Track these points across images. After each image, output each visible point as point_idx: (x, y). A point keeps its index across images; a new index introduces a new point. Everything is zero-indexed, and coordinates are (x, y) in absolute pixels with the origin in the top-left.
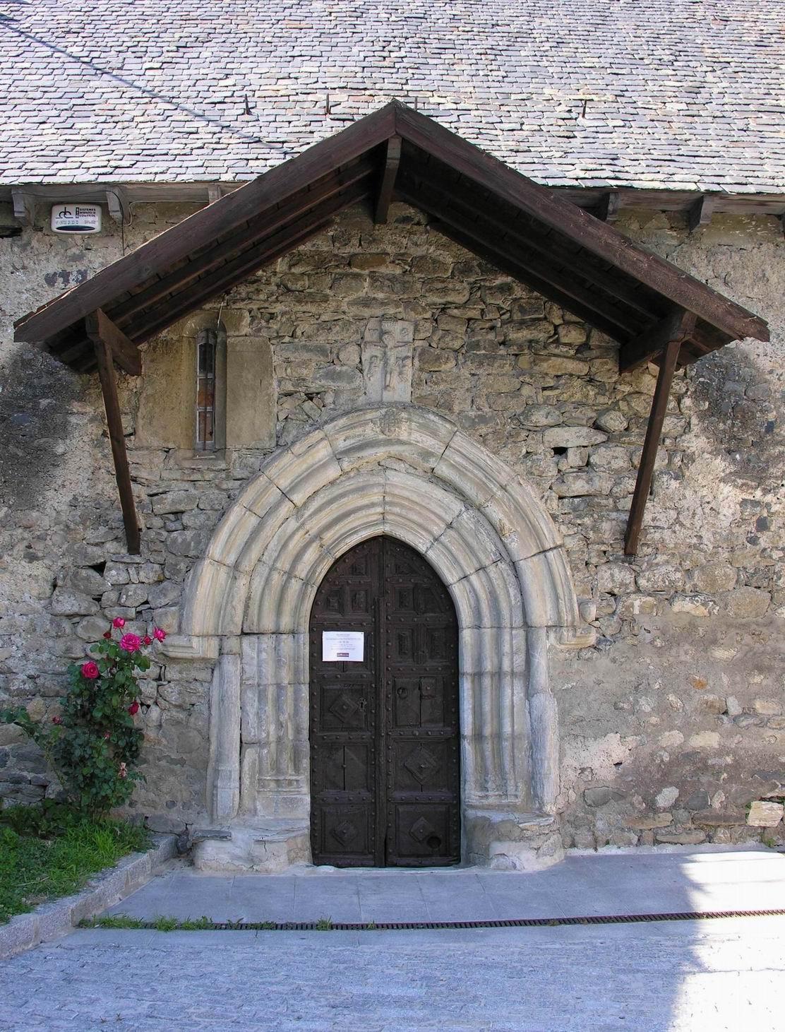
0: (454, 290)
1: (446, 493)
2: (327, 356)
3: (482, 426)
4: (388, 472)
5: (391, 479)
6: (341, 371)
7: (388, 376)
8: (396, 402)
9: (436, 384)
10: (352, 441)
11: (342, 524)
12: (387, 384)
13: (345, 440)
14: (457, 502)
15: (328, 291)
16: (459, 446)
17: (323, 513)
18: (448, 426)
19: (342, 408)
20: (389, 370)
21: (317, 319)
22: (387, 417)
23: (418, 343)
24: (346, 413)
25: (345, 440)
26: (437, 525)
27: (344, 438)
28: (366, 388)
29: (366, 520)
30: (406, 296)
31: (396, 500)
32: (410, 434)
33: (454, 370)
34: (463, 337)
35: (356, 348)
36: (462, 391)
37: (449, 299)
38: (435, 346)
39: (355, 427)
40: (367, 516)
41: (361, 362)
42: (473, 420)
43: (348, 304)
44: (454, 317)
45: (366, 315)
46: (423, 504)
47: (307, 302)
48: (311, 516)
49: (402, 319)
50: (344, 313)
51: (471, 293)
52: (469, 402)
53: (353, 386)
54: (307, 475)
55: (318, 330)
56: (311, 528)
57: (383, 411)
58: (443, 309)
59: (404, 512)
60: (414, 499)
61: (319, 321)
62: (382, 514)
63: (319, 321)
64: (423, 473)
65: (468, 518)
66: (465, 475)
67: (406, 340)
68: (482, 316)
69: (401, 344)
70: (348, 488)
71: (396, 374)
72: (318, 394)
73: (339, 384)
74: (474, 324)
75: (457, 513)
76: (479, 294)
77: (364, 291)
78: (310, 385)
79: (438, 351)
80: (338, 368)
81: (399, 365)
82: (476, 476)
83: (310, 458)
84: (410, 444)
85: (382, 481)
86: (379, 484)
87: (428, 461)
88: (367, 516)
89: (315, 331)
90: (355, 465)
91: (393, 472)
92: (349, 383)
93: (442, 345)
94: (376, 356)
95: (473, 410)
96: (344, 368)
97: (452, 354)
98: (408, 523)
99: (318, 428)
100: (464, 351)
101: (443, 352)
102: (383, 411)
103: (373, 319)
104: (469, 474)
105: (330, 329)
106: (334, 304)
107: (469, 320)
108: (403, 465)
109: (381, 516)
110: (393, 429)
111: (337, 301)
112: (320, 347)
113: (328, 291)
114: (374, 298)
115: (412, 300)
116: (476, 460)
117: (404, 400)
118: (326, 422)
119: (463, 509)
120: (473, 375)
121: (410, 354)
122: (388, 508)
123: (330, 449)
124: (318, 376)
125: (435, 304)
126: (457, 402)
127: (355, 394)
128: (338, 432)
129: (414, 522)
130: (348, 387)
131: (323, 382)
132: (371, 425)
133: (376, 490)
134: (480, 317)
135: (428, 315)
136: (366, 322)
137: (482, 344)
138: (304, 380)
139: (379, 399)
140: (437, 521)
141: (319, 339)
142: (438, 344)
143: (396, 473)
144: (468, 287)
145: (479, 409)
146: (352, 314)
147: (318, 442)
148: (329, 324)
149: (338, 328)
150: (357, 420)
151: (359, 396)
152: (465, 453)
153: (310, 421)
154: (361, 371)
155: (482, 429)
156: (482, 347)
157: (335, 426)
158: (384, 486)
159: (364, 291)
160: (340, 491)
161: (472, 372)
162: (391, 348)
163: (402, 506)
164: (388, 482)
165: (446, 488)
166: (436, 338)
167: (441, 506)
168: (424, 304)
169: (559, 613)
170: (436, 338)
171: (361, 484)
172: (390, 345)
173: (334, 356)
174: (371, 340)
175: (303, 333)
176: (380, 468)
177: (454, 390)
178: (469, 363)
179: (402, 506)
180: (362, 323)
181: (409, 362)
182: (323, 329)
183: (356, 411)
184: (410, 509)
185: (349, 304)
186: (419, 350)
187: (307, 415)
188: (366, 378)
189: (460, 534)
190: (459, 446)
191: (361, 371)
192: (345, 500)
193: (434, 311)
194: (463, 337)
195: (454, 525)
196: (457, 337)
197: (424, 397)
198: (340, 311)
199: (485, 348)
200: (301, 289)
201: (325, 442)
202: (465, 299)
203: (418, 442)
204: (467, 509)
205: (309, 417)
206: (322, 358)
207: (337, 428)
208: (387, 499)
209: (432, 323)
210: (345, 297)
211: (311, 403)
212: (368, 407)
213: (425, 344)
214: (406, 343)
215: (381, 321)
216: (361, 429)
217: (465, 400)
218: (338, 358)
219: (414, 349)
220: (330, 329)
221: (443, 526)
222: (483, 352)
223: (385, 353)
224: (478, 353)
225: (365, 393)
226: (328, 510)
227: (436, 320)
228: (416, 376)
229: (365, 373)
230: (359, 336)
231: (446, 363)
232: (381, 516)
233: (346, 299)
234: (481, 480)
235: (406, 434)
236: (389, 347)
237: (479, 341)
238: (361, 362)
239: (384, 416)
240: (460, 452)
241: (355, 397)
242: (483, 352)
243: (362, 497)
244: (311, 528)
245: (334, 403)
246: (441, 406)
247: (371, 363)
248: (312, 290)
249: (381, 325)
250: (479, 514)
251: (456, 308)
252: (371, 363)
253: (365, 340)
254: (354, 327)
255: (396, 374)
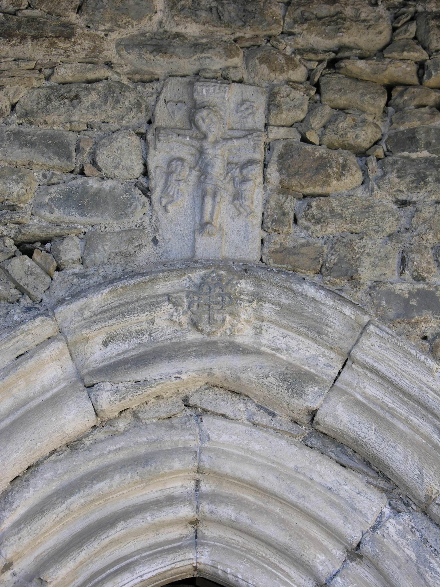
0: (356, 19)
1: (344, 472)
2: (69, 157)
3: (427, 314)
4: (207, 422)
5: (214, 436)
6: (98, 193)
7: (209, 200)
8: (226, 260)
9: (318, 221)
10: (123, 346)
11: (94, 546)
12: (207, 218)
13: (105, 344)
14: (369, 493)
15: (73, 17)
16: (375, 359)
17: (49, 519)
18: (347, 311)
19: (102, 272)
20: (209, 188)
21: (48, 78)
22: (205, 289)
23: (275, 133)
24: (108, 281)
25: (105, 344)
26: (325, 550)
27: (102, 337)
28: (156, 230)
29: (152, 539)
30: (248, 33)
31: (227, 490)
32: (258, 331)
33: (360, 192)
34: (379, 123)
35: (136, 140)
36: (379, 239)
37: (346, 39)
38: (313, 137)
39: (129, 312)
40: (157, 527)
41: (145, 174)
42: (407, 301)
43: (118, 45)
44: (357, 79)
45: (160, 72)
46: (292, 498)
47: (24, 37)
48: (18, 525)
49: (241, 82)
50: (109, 64)
51: (394, 29)
52: (394, 261)
53: (128, 223)
54: (14, 423)
55: (49, 100)
56: (20, 556)
57: (196, 276)
58: (333, 64)
59: (245, 518)
60: (266, 484)
61: (53, 82)
62: (194, 523)
63: (53, 82)
64: (291, 425)
65: (398, 532)
66: (390, 427)
67: (250, 123)
68: (420, 78)
69: (236, 133)
70: (111, 459)
71: (225, 197)
72: (44, 242)
73: (95, 220)
74: (401, 94)
75: (371, 520)
76: (413, 28)
77: (156, 18)
78: (26, 219)
79: (322, 151)
80: (93, 184)
81: (233, 179)
82: (416, 429)
83: (22, 383)
84: (259, 353)
85: (193, 443)
86: (186, 450)
87: (301, 394)
88: (157, 527)
89: (43, 103)
90: (125, 404)
91: (220, 422)
92: (118, 218)
93: (330, 137)
94: (181, 160)
95: (404, 281)
96: (108, 184)
97: (353, 159)
98: (254, 546)
99: (41, 315)
100: (380, 151)
101: (334, 153)
102: (196, 276)
103: (174, 80)
104: (400, 426)
105: (77, 97)
106: (87, 44)
107: (389, 88)
108: (241, 406)
109: (190, 530)
110: (218, 317)
111: (94, 38)
112: (52, 137)
113: (73, 17)
114: (178, 35)
115: (263, 43)
116: (415, 392)
117: (245, 257)
118: (62, 301)
119: (387, 511)
120: (403, 204)
121: (259, 156)
122: (206, 507)
123: (70, 366)
124: (46, 199)
125: (314, 51)
126: (367, 261)
127: (131, 241)
128: (90, 323)
129: (268, 543)
130: (115, 226)
131: (58, 214)
132: (168, 307)
133: (177, 465)
134: (415, 80)
135: (299, 74)
136: (157, 85)
137: (421, 136)
138: (13, 208)
139: (186, 253)
140: (326, 542)
141: (50, 119)
142: (321, 137)
143: (225, 423)
144: (387, 15)
145: (418, 278)
146: (127, 69)
147: (41, 346)
148: (74, 87)
149: (94, 97)
150: (133, 295)
151: (140, 247)
152: (389, 374)
153: (26, 302)
154: (146, 191)
155: (426, 321)
156: (422, 143)
157: (81, 310)
158: (196, 454)
159: (156, 18)
160: (92, 466)
161: (402, 197)
162: (216, 142)
163: (240, 504)
164: (207, 445)
165: (344, 460)
166: (316, 122)
167: (332, 504)
168: (289, 51)
169: (343, 545)
170: (316, 122)
171: (142, 451)
172: (214, 132)
173: (85, 157)
174: (172, 124)
175: (13, 107)
176: (189, 412)
177: (361, 236)
178: (393, 176)
179: (240, 504)
180: (149, 88)
181: (256, 171)
182: (61, 97)
183: (132, 277)
184: (261, 511)
185: (120, 45)
186: (279, 147)
187: (18, 287)
188: (157, 206)
189: (381, 574)
190: (375, 359)
191: (146, 191)
192: (102, 486)
193: (313, 65)
194: (379, 123)
195: (367, 549)
196: (364, 121)
197: (293, 251)
198: (101, 61)
199: (428, 146)
200: (11, 9)
201: (58, 346)
202: (385, 37)
203: (277, 350)
204: (397, 511)
205: (23, 291)
206: (56, 161)
207: (87, 314)
208: (205, 487)
209: (307, 90)
210: (111, 30)
211: (28, 261)
212: (161, 267)
213: (295, 137)
214: (250, 132)
215: (191, 84)
216: (143, 317)
217: (387, 257)
218: (94, 163)
219: (269, 148)
220: (77, 97)
221: (339, 553)
222: (425, 154)
223: (201, 152)
224: (414, 155)
225: (155, 241)
226: (60, 511)
227: (317, 85)
228: (273, 203)
229: (155, 196)
230: (142, 117)
231: (340, 176)
232: (190, 530)
233: (114, 36)
234: (428, 439)
235: (249, 330)
236: (211, 138)
237: (413, 131)
238: (145, 174)
239: (200, 287)
240: (377, 373)
241: (131, 249)
242: (425, 154)
243: (146, 481)
244: (20, 556)
245: (82, 261)
246: (330, 271)
247: (169, 174)
248: (36, 13)
249: (193, 91)
250: (426, 523)
251: (361, 58)
252: (169, 174)
253: (156, 124)
254: (130, 97)
255: (225, 197)
